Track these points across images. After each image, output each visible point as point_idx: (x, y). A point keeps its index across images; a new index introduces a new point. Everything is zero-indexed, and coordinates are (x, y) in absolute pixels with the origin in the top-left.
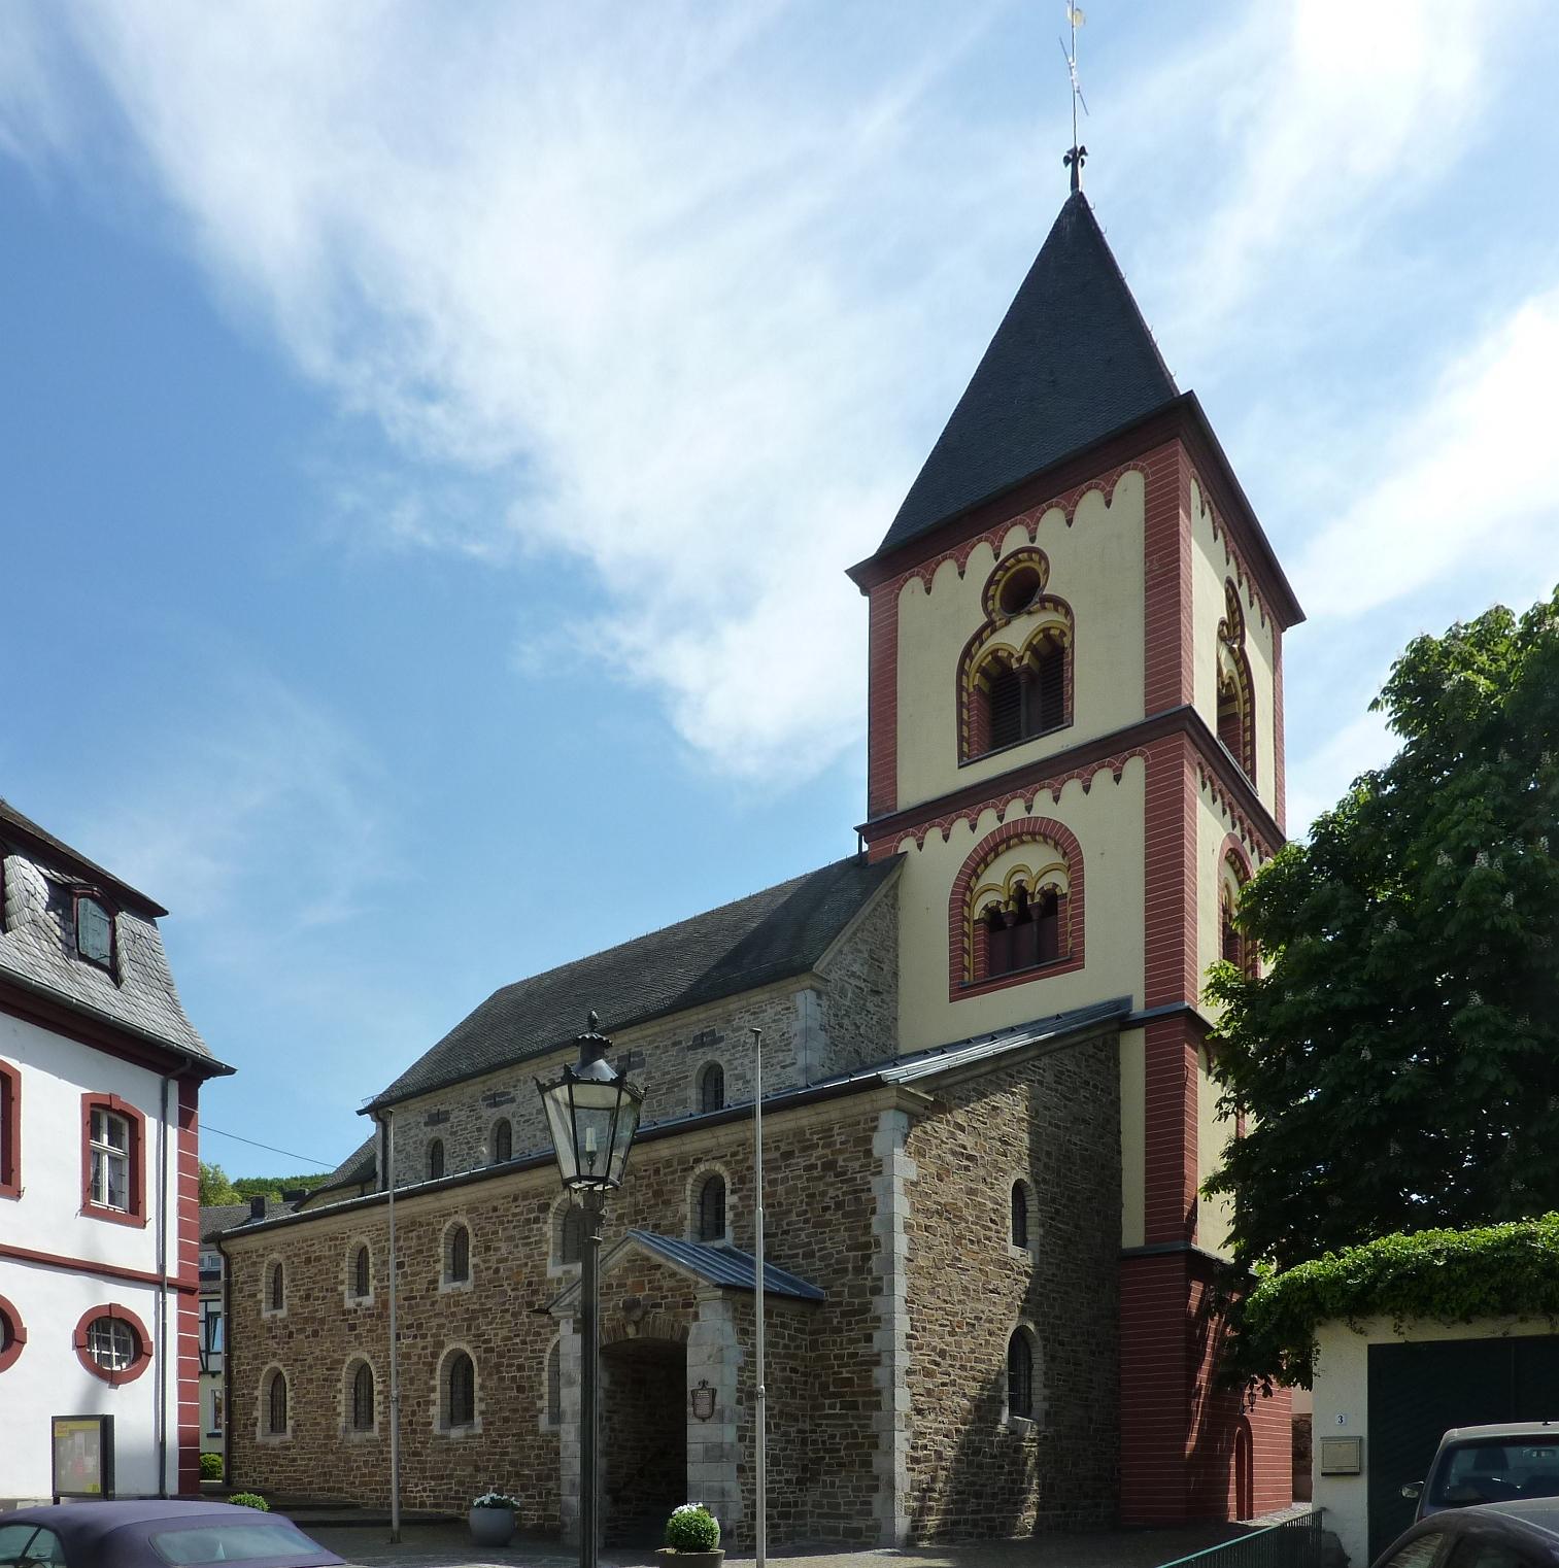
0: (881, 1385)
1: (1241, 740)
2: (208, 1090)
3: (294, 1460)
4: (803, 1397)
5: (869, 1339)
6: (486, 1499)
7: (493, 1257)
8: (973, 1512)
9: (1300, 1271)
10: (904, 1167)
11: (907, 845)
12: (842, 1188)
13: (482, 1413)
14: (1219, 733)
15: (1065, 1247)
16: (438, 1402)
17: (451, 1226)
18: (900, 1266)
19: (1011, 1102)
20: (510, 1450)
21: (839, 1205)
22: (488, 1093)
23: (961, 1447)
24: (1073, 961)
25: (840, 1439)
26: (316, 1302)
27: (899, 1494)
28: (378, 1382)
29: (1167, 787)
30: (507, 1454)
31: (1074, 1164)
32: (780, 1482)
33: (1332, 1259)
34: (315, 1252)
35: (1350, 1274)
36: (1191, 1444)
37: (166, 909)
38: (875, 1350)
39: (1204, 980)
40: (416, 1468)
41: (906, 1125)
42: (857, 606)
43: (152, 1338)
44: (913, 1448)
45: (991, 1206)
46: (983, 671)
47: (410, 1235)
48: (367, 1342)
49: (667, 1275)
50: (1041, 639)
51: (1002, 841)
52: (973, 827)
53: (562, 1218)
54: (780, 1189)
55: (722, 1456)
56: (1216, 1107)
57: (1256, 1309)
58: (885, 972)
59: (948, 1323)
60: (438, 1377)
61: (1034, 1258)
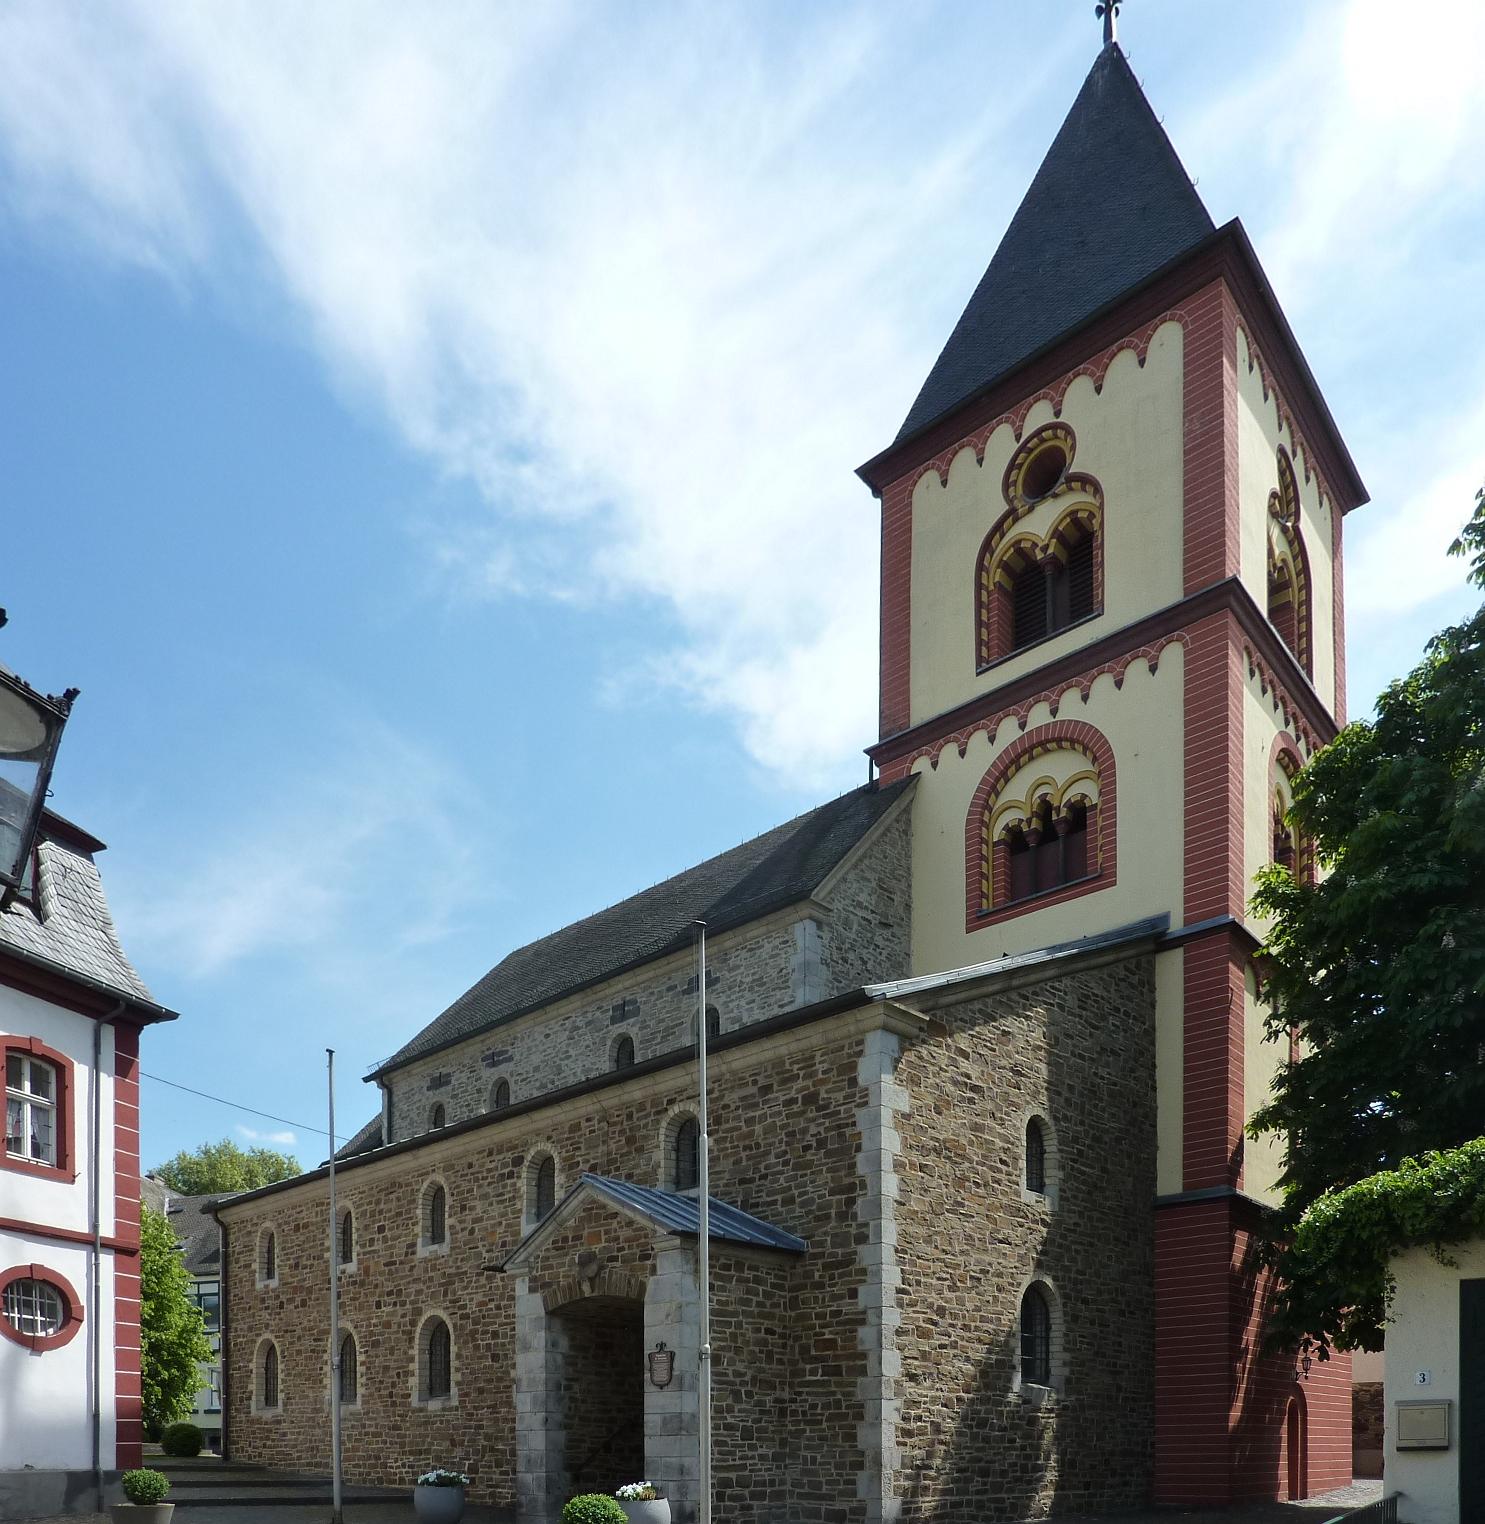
0: (867, 1346)
1: (1296, 632)
2: (150, 1036)
3: (285, 1434)
4: (780, 1362)
5: (853, 1294)
6: (432, 1476)
7: (469, 1216)
8: (978, 1492)
9: (1370, 1183)
10: (893, 1096)
11: (921, 765)
12: (824, 1123)
13: (458, 1384)
14: (1271, 612)
15: (1089, 1193)
16: (417, 1372)
17: (429, 1186)
18: (888, 1210)
19: (1026, 1028)
20: (484, 1423)
21: (821, 1143)
22: (487, 1053)
23: (964, 1418)
24: (1104, 878)
25: (822, 1409)
26: (305, 1271)
27: (887, 1472)
28: (361, 1353)
29: (1209, 673)
30: (481, 1427)
31: (1101, 1100)
32: (753, 1457)
33: (1413, 1167)
34: (303, 1219)
35: (1437, 1184)
36: (1235, 1414)
37: (102, 842)
38: (861, 1307)
39: (1252, 888)
40: (396, 1443)
41: (896, 1048)
42: (869, 508)
43: (83, 1301)
44: (904, 1419)
45: (1001, 1144)
46: (1005, 566)
47: (391, 1196)
48: (350, 1311)
49: (623, 1224)
50: (1068, 524)
51: (1025, 752)
52: (992, 739)
53: (537, 1171)
54: (758, 1128)
55: (681, 1429)
56: (1265, 1025)
57: (1310, 1235)
58: (896, 903)
59: (948, 1276)
60: (416, 1347)
61: (1052, 1204)
